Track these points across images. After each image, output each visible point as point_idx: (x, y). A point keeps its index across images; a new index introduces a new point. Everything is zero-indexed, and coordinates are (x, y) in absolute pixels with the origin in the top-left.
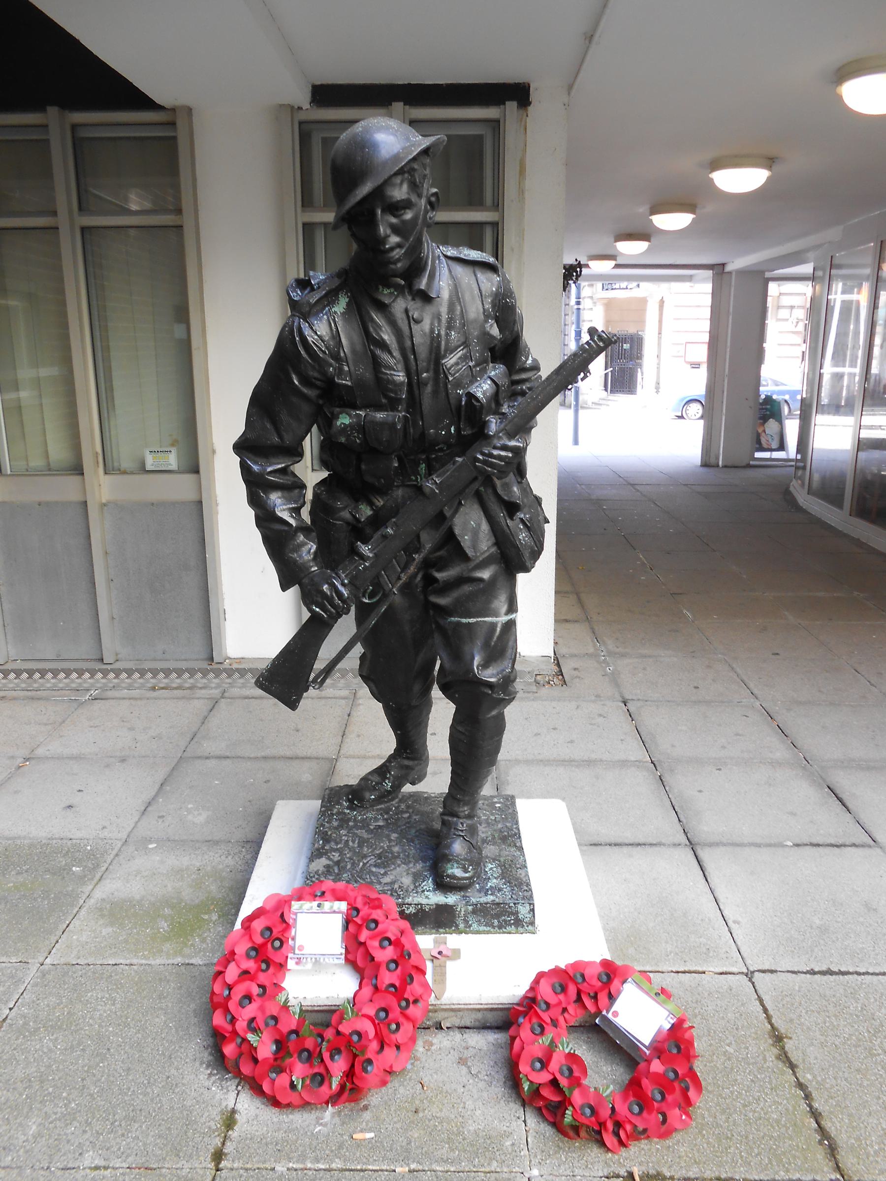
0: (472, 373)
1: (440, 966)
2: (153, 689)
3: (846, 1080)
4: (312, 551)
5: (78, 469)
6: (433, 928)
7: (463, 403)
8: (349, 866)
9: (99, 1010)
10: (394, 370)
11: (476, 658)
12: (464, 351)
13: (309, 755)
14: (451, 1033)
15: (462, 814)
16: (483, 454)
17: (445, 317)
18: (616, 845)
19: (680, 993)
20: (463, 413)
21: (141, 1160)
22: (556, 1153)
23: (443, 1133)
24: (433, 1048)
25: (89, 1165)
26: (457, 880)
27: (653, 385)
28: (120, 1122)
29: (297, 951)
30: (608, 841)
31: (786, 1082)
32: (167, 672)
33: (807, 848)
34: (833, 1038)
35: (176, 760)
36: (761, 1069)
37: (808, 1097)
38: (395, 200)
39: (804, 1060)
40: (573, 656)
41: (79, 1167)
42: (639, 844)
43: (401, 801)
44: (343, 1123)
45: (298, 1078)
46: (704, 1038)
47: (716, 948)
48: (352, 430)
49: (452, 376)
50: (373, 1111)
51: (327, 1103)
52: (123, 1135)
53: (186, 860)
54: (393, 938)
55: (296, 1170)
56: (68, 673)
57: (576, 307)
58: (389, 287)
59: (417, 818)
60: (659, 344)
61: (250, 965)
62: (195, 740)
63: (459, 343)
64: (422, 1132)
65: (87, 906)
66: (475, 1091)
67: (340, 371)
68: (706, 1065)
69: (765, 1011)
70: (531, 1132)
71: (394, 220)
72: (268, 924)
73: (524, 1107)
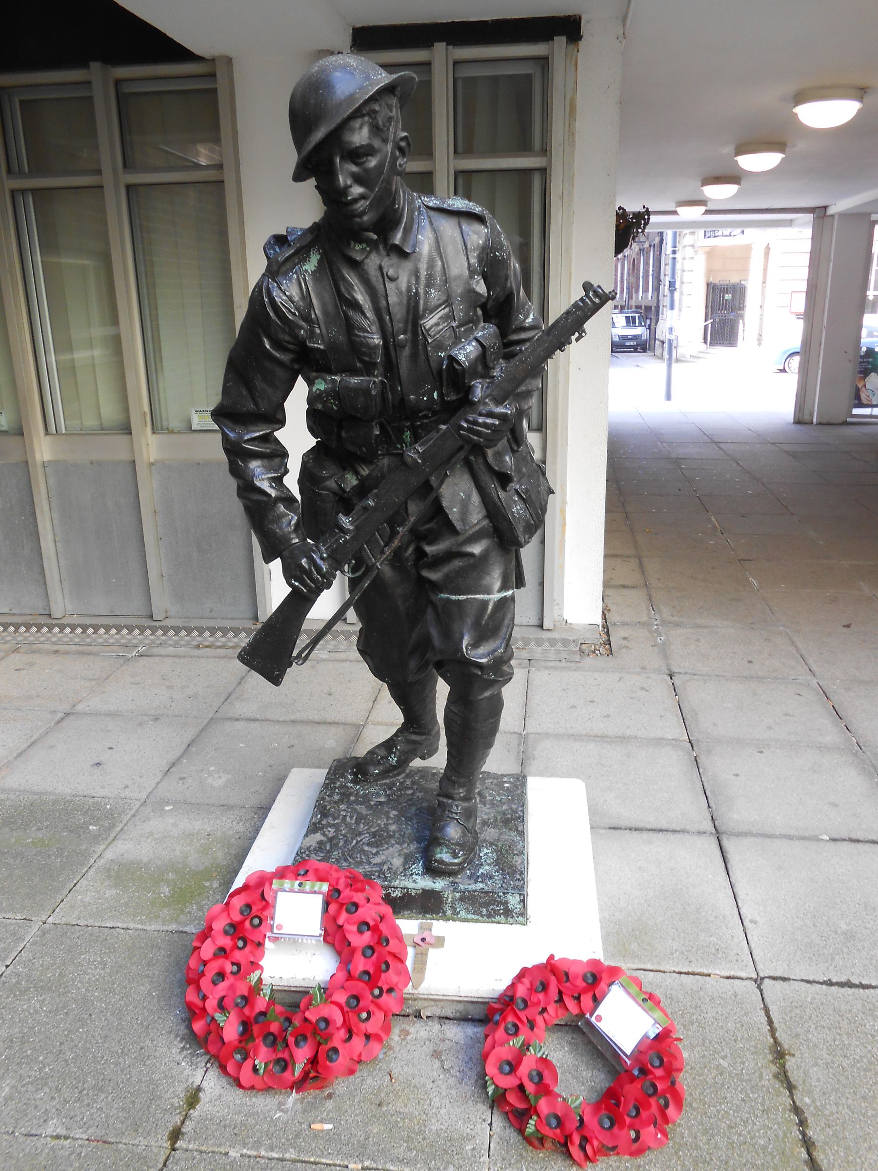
0: (455, 334)
1: (422, 954)
2: (198, 647)
3: (849, 1107)
4: (293, 522)
5: (127, 429)
6: (420, 913)
7: (444, 367)
8: (341, 844)
9: (88, 974)
10: (368, 332)
11: (466, 638)
12: (447, 310)
13: (337, 720)
14: (430, 1023)
15: (457, 797)
16: (467, 421)
17: (423, 273)
18: (636, 830)
19: (680, 996)
20: (444, 378)
21: (100, 1133)
22: (517, 1162)
23: (404, 1131)
24: (409, 1038)
25: (51, 1133)
26: (445, 865)
27: (756, 337)
28: (88, 1091)
29: (275, 931)
30: (629, 825)
31: (780, 1104)
32: (213, 631)
33: (845, 843)
34: (841, 1059)
35: (206, 721)
36: (754, 1089)
37: (802, 1123)
38: (353, 146)
39: (804, 1081)
40: (624, 624)
41: (41, 1135)
42: (661, 830)
43: (407, 776)
44: (305, 1111)
45: (260, 1062)
46: (697, 1048)
47: (727, 948)
48: (327, 396)
49: (432, 337)
50: (336, 1100)
51: (292, 1088)
52: (88, 1105)
53: (198, 824)
54: (372, 923)
55: (249, 1157)
56: (119, 629)
57: (671, 256)
58: (361, 243)
59: (420, 795)
60: (763, 294)
61: (226, 942)
62: (229, 700)
63: (441, 301)
64: (382, 1128)
65: (96, 867)
66: (444, 1087)
67: (312, 333)
68: (694, 1079)
69: (770, 1022)
70: (495, 1137)
71: (354, 168)
72: (249, 900)
73: (492, 1108)
